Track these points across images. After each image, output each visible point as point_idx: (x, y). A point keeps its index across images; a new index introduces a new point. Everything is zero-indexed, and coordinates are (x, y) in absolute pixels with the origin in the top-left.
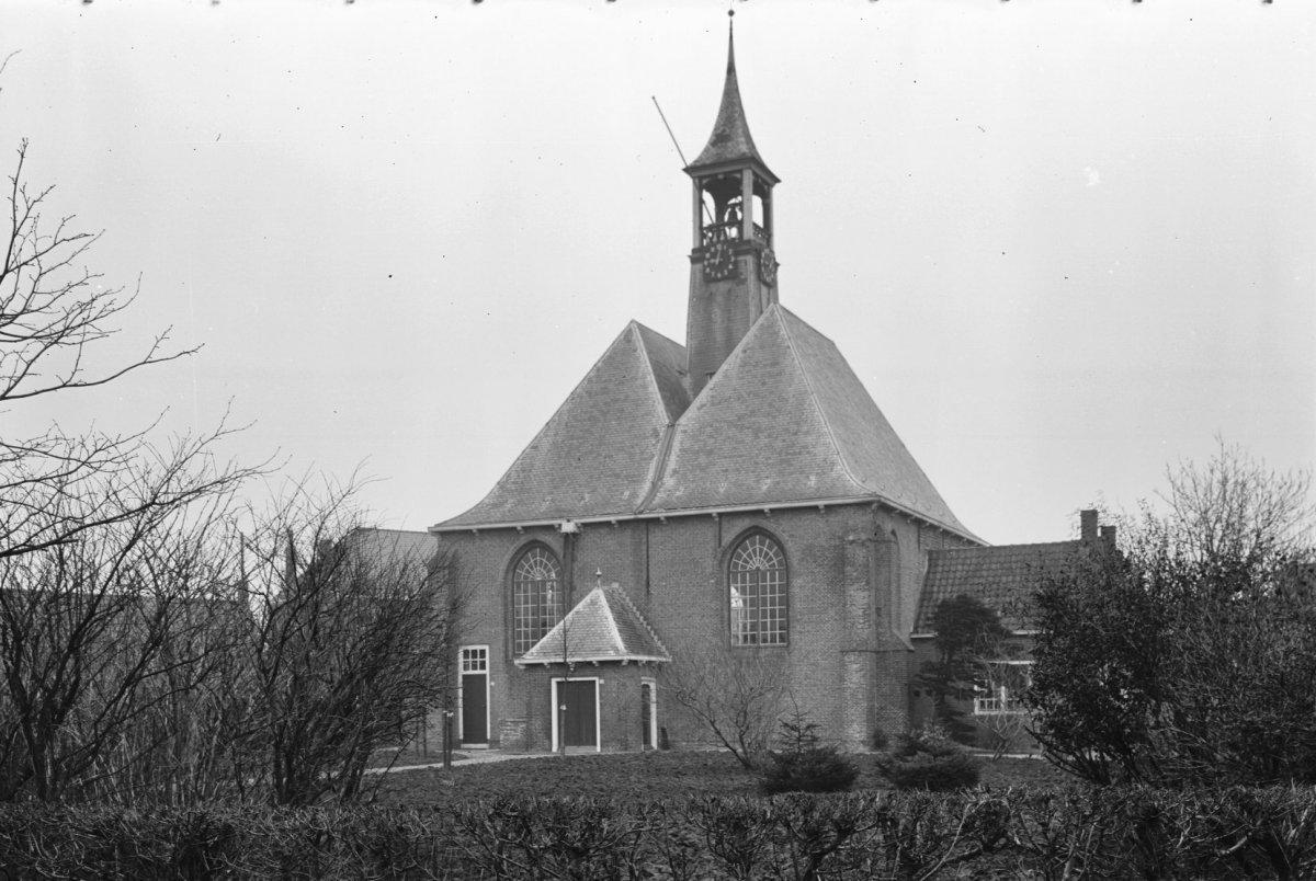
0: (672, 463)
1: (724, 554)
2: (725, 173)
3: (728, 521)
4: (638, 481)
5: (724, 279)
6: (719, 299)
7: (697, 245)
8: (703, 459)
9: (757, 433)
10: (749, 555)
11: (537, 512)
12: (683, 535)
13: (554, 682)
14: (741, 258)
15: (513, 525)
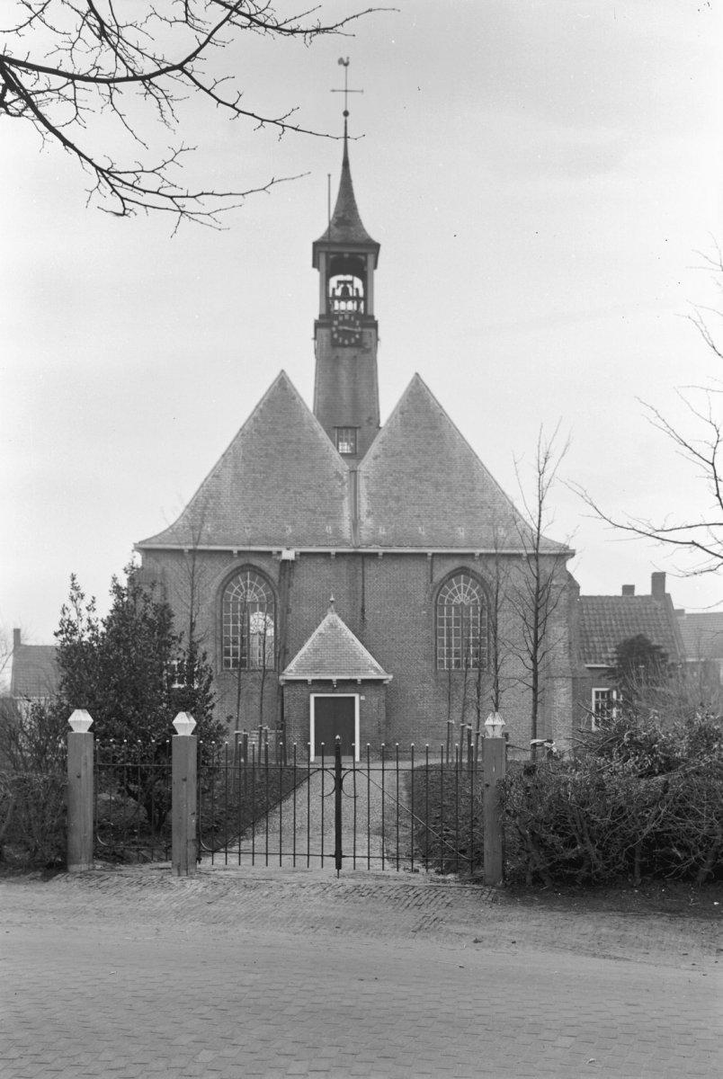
0: (364, 506)
1: (435, 588)
2: (351, 254)
3: (439, 561)
4: (336, 518)
5: (351, 345)
6: (346, 362)
7: (324, 312)
8: (392, 504)
9: (437, 486)
10: (454, 591)
11: (239, 533)
12: (397, 570)
13: (312, 697)
14: (365, 330)
15: (229, 548)
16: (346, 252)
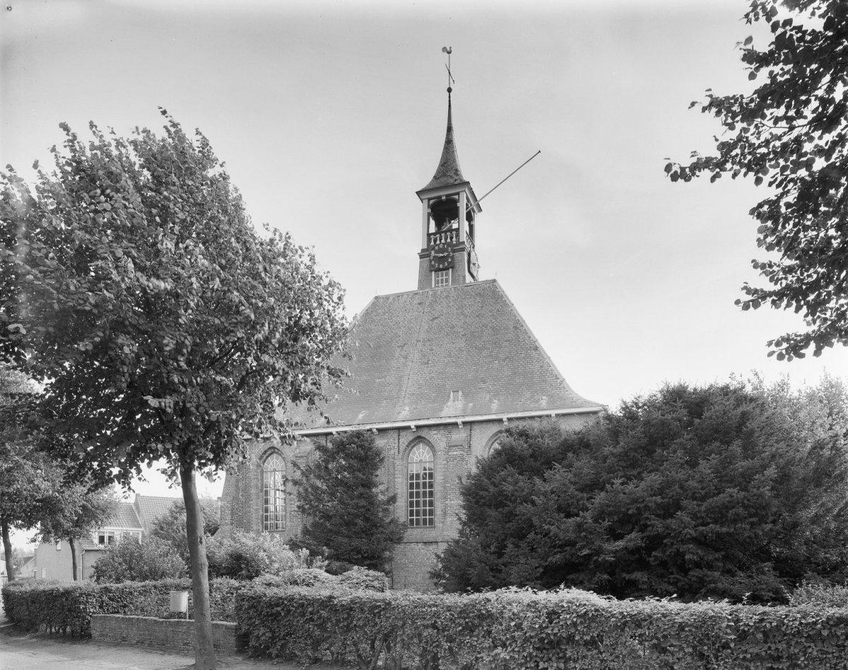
2: (447, 196)
16: (445, 204)
